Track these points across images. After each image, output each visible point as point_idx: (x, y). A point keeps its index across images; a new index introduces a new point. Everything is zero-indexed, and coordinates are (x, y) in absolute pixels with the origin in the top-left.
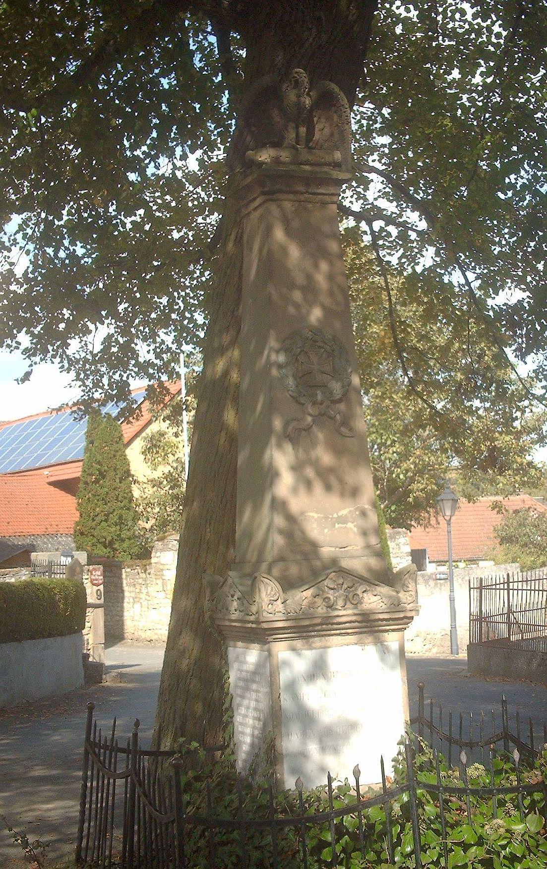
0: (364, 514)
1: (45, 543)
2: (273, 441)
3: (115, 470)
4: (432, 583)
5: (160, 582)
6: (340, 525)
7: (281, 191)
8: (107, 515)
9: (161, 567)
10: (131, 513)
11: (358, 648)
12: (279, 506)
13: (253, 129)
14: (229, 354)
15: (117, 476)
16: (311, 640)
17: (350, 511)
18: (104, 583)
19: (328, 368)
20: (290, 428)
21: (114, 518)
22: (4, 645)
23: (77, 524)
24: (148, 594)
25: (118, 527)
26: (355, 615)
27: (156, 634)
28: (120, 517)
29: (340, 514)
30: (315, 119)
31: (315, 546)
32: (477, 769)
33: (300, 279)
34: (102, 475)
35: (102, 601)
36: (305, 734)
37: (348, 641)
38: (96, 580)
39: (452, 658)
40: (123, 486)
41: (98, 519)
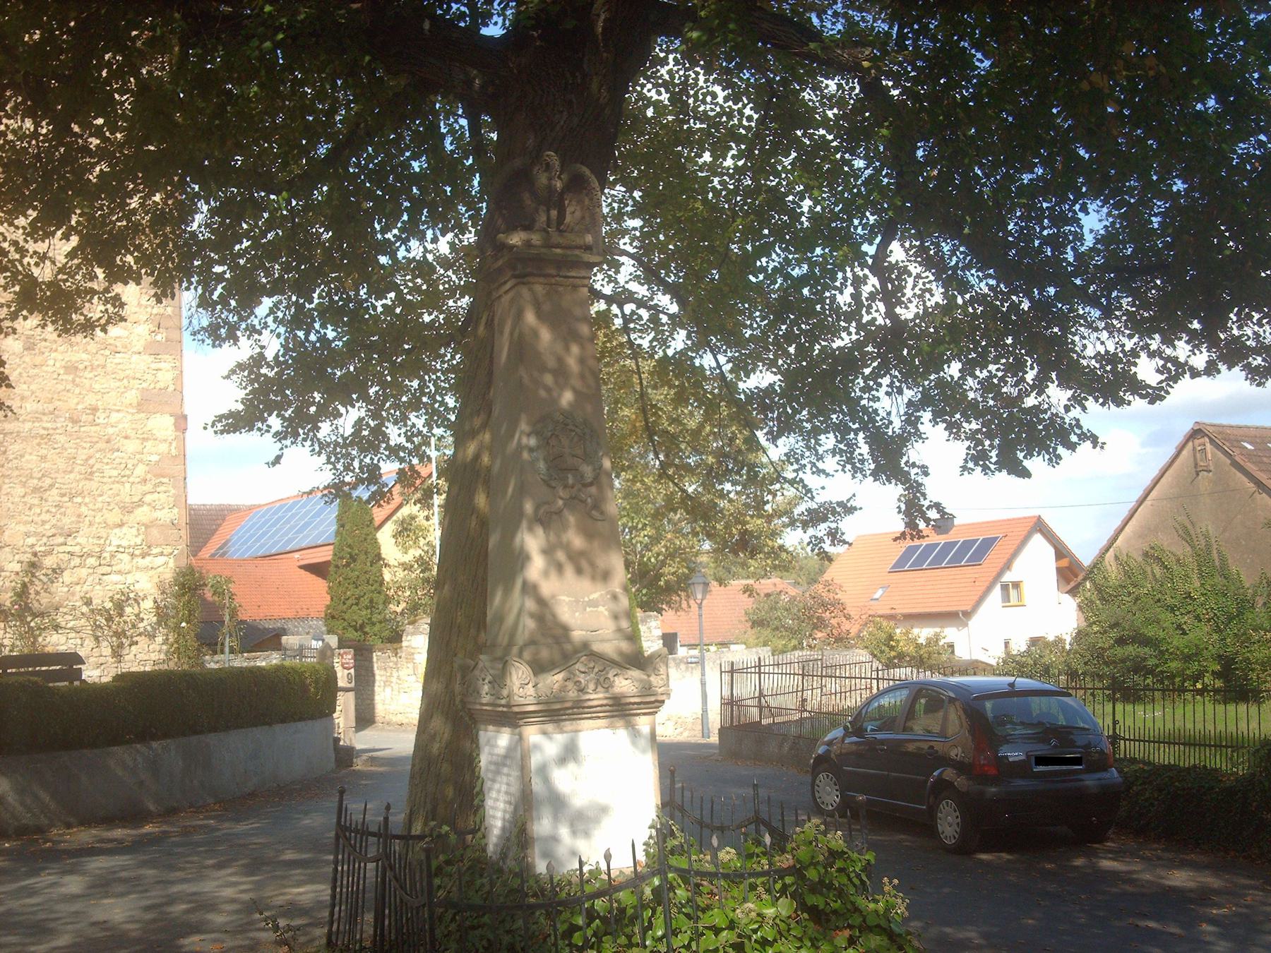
0: (615, 597)
1: (296, 627)
2: (524, 524)
3: (366, 553)
4: (683, 666)
5: (410, 665)
8: (358, 599)
10: (382, 597)
12: (530, 589)
13: (504, 212)
14: (480, 437)
19: (579, 452)
21: (365, 601)
22: (254, 729)
23: (328, 607)
25: (369, 611)
28: (371, 601)
30: (566, 202)
31: (566, 629)
33: (551, 363)
34: (353, 558)
35: (353, 685)
36: (556, 818)
40: (374, 569)
41: (349, 602)
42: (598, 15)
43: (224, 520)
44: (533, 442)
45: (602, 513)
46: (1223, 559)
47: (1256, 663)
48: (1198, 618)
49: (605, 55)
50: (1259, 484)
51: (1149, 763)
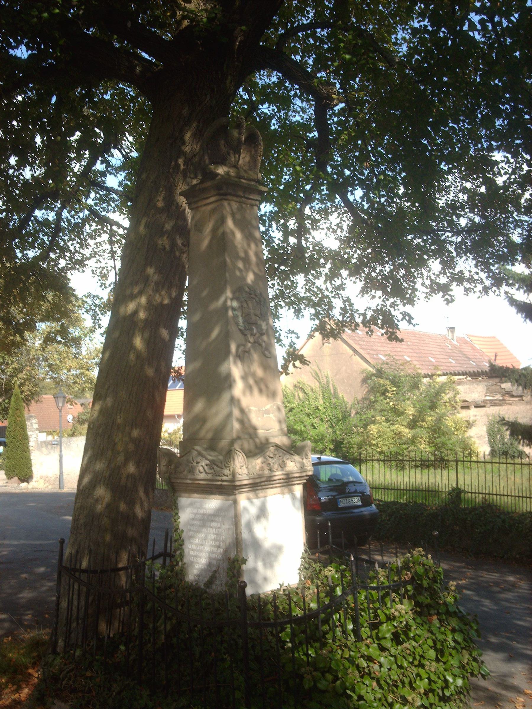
0: (279, 409)
2: (231, 359)
4: (49, 447)
7: (230, 194)
11: (280, 496)
12: (234, 401)
13: (209, 151)
14: (138, 300)
16: (257, 492)
19: (258, 312)
20: (240, 350)
26: (283, 474)
31: (255, 429)
32: (330, 571)
33: (242, 254)
36: (256, 557)
39: (60, 491)
42: (237, 38)
44: (235, 304)
45: (270, 353)
46: (335, 390)
47: (354, 444)
48: (322, 420)
49: (236, 63)
50: (355, 351)
51: (381, 501)
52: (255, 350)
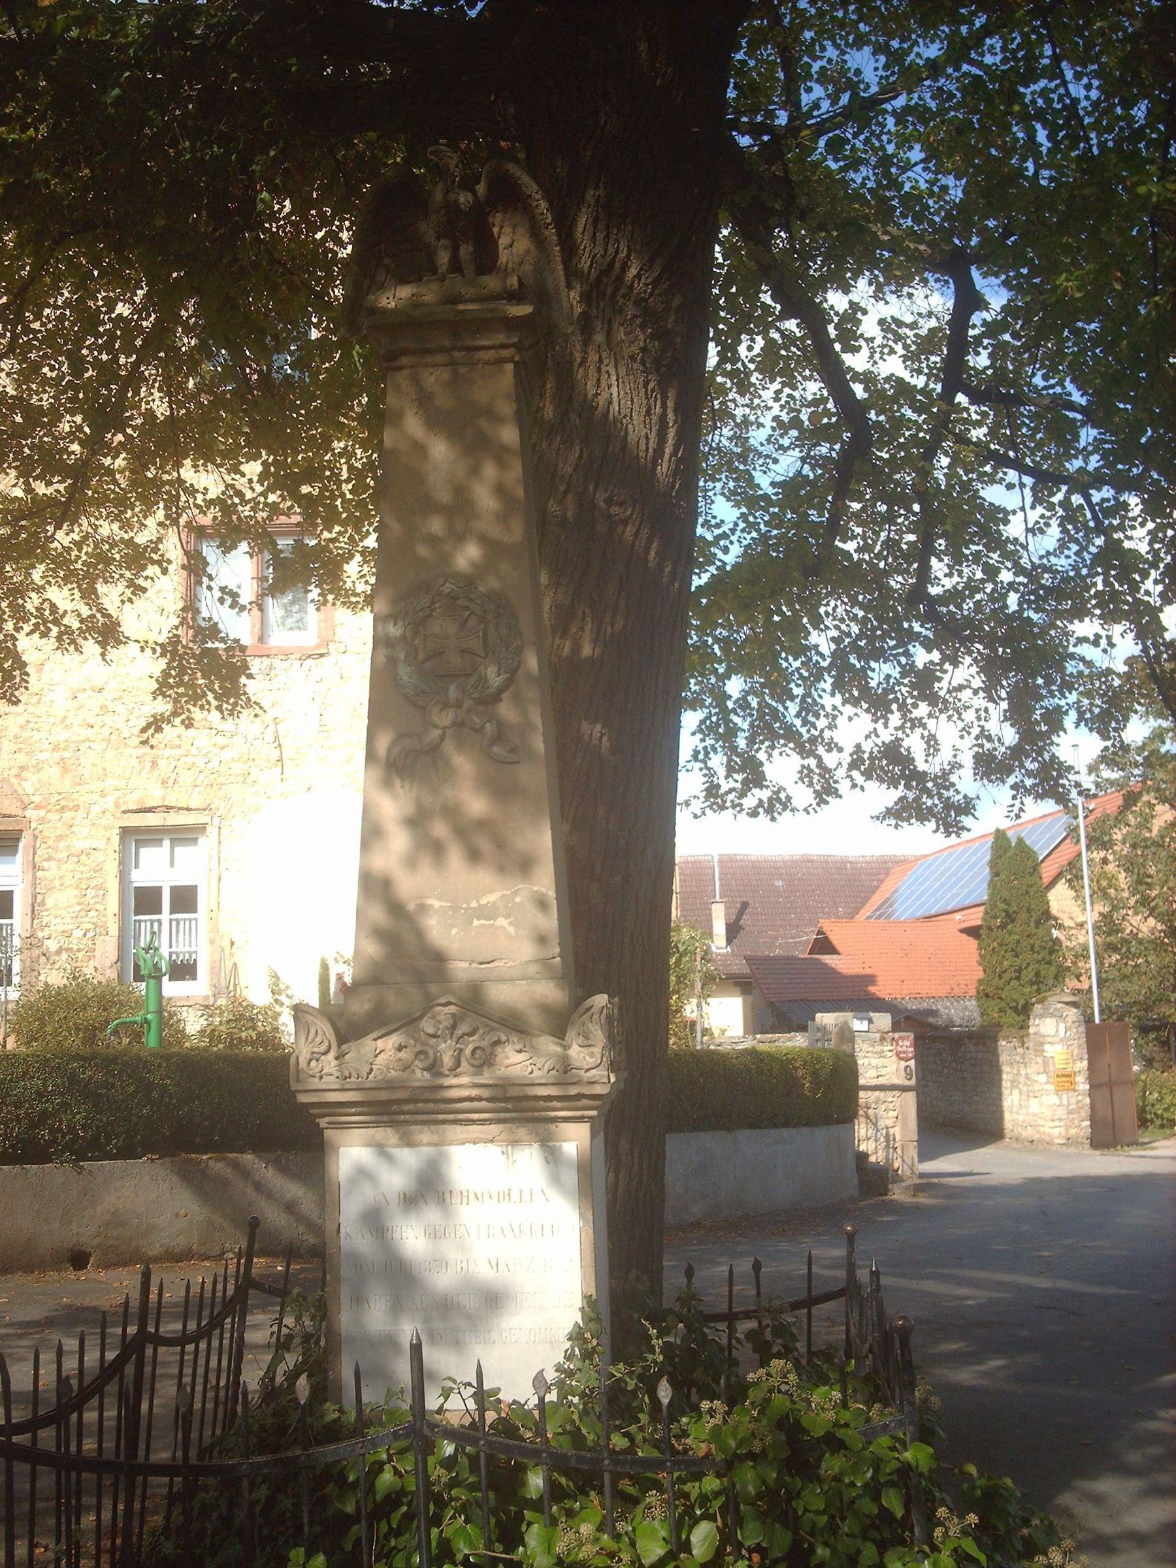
1: (946, 1008)
3: (1029, 910)
5: (1040, 1060)
6: (483, 922)
8: (1019, 971)
9: (1041, 1040)
10: (1053, 969)
15: (1033, 919)
17: (504, 895)
18: (915, 1057)
21: (1028, 974)
22: (703, 1134)
23: (980, 982)
24: (1027, 1077)
25: (1035, 987)
27: (1038, 1132)
28: (1037, 974)
29: (483, 901)
30: (495, 230)
31: (439, 958)
34: (1010, 917)
35: (913, 1082)
36: (397, 1308)
37: (474, 1135)
38: (904, 1052)
40: (1041, 932)
41: (1006, 976)
43: (887, 874)
52: (461, 744)
